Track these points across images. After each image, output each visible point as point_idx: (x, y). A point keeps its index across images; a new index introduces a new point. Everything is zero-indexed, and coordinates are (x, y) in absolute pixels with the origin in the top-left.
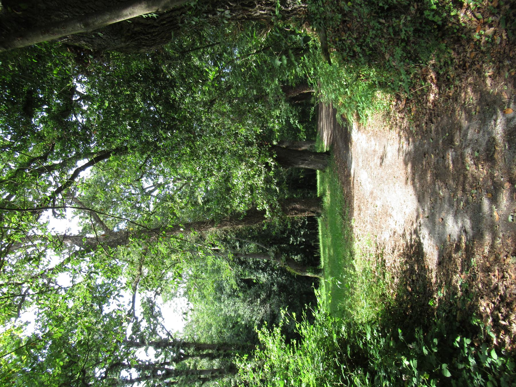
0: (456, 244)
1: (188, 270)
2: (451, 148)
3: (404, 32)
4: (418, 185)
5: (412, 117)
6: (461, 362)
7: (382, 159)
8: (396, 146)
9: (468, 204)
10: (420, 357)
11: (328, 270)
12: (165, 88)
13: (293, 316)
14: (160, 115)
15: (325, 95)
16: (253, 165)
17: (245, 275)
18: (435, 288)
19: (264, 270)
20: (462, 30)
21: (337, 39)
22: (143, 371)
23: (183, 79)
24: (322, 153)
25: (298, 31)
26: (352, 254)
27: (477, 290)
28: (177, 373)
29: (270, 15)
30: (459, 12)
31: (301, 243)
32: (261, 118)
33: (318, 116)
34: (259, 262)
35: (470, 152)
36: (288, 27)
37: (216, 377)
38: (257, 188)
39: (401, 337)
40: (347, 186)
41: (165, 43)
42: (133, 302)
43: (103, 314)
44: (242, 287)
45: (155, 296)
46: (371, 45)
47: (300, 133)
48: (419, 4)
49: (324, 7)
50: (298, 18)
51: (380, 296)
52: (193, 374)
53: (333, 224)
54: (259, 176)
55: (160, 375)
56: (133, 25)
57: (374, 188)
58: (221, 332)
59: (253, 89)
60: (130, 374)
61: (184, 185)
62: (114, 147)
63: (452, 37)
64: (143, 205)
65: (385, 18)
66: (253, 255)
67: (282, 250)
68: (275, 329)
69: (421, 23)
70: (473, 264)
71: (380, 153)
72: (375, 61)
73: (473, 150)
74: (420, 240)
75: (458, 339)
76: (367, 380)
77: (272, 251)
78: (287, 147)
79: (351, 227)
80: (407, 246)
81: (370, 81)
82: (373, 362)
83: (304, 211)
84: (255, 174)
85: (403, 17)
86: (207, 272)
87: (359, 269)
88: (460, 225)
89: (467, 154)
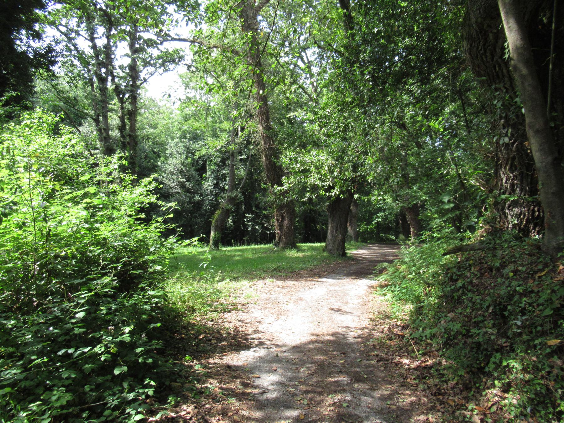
0: (250, 384)
1: (215, 101)
2: (351, 380)
3: (477, 332)
4: (311, 346)
5: (383, 341)
6: (130, 385)
7: (338, 310)
8: (352, 325)
9: (293, 396)
10: (133, 345)
11: (218, 254)
12: (420, 73)
13: (169, 214)
14: (390, 67)
15: (409, 251)
16: (332, 172)
17: (210, 165)
18: (203, 362)
19: (216, 185)
20: (478, 392)
21: (471, 262)
22: (104, 52)
23: (430, 93)
24: (344, 248)
25: (481, 219)
26: (236, 279)
27: (204, 403)
28: (103, 90)
29: (501, 189)
30: (497, 389)
31: (246, 226)
32: (384, 181)
33: (384, 244)
34: (225, 180)
35: (347, 398)
36: (486, 210)
37: (101, 134)
38: (306, 177)
39: (152, 326)
40: (308, 274)
41: (473, 70)
42: (180, 40)
43: (166, 5)
44: (197, 161)
45: (186, 65)
46: (464, 297)
47: (366, 225)
48: (508, 348)
49: (508, 247)
50: (496, 220)
51: (192, 307)
52: (103, 107)
53: (267, 260)
54: (320, 179)
55: (100, 71)
56: (495, 31)
57: (307, 302)
58: (148, 138)
59: (417, 171)
60: (100, 37)
61: (309, 96)
62: (354, 14)
63: (470, 382)
64: (287, 49)
65: (494, 313)
66: (233, 174)
67: (238, 206)
68: (155, 196)
69: (487, 350)
70: (230, 399)
71: (343, 308)
72: (446, 302)
73: (349, 402)
74: (253, 347)
75: (152, 383)
76: (107, 290)
77: (237, 194)
78: (351, 210)
79: (264, 279)
80: (246, 335)
81: (423, 297)
82: (125, 297)
83: (281, 228)
84: (321, 175)
85: (495, 331)
86: (213, 123)
87: (220, 286)
88: (270, 387)
89: (344, 395)
